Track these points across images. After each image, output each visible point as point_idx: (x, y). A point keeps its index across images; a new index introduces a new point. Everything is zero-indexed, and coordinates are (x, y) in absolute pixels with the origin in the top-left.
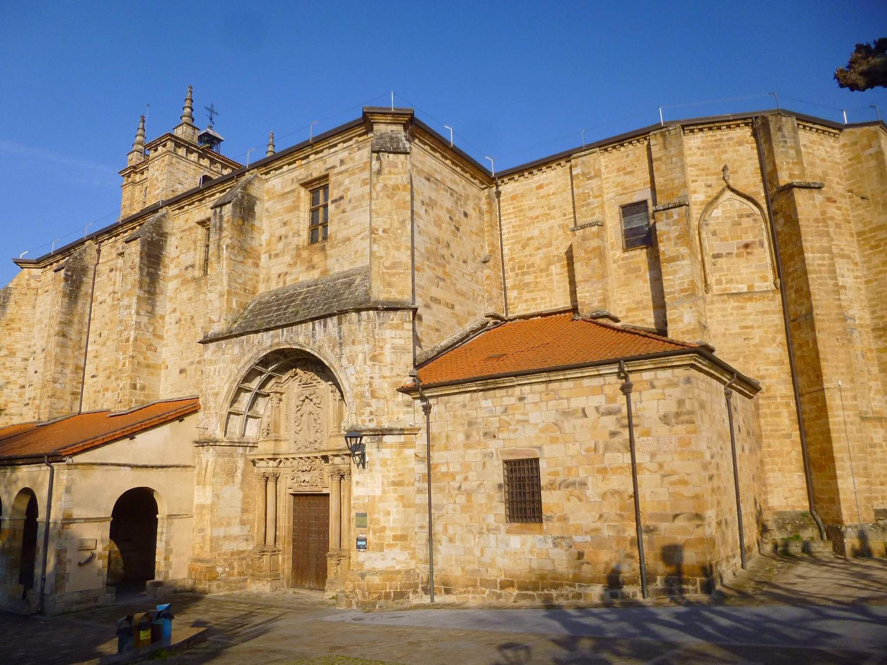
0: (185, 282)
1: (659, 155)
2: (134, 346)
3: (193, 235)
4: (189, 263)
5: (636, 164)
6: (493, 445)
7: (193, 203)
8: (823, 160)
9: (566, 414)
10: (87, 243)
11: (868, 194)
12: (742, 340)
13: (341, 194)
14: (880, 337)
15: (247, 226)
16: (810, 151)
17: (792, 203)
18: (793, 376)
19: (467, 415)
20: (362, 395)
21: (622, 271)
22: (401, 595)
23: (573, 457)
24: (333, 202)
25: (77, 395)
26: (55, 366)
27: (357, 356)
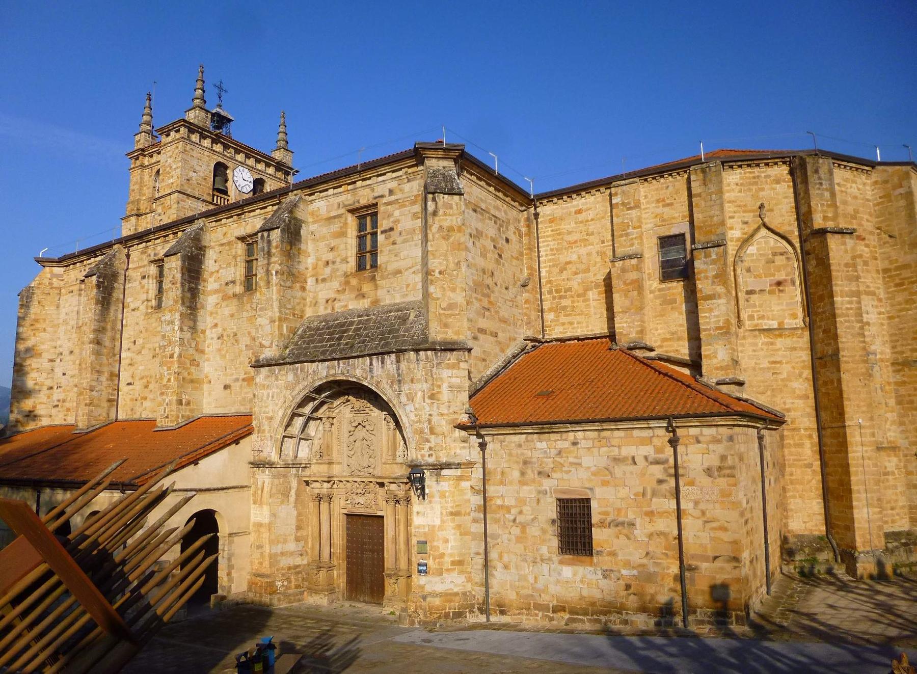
0: (225, 298)
1: (699, 191)
2: (179, 362)
3: (233, 251)
4: (230, 279)
5: (675, 196)
6: (547, 484)
7: (231, 217)
8: (855, 198)
9: (617, 460)
10: (115, 247)
11: (896, 234)
12: (770, 374)
13: (391, 225)
14: (898, 371)
15: (294, 251)
16: (843, 189)
17: (825, 247)
18: (816, 410)
19: (522, 454)
20: (422, 432)
21: (658, 302)
22: (459, 614)
23: (622, 499)
24: (382, 232)
25: (113, 402)
26: (92, 374)
27: (416, 393)
